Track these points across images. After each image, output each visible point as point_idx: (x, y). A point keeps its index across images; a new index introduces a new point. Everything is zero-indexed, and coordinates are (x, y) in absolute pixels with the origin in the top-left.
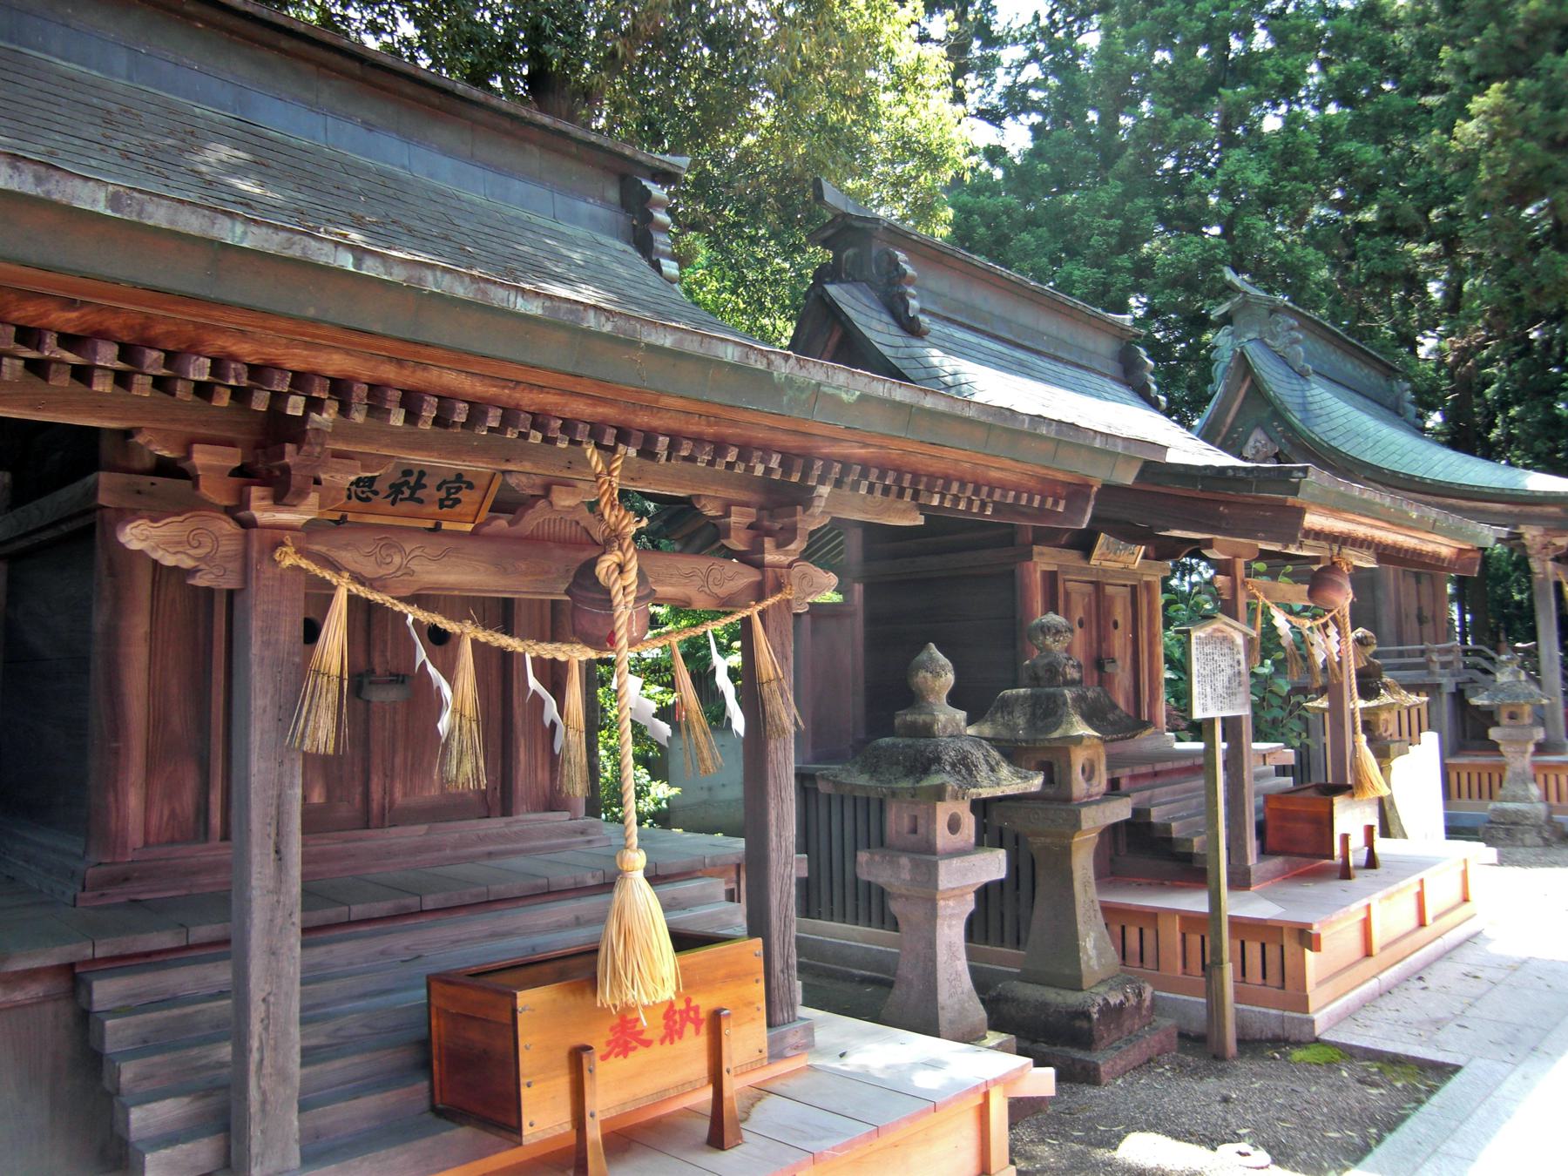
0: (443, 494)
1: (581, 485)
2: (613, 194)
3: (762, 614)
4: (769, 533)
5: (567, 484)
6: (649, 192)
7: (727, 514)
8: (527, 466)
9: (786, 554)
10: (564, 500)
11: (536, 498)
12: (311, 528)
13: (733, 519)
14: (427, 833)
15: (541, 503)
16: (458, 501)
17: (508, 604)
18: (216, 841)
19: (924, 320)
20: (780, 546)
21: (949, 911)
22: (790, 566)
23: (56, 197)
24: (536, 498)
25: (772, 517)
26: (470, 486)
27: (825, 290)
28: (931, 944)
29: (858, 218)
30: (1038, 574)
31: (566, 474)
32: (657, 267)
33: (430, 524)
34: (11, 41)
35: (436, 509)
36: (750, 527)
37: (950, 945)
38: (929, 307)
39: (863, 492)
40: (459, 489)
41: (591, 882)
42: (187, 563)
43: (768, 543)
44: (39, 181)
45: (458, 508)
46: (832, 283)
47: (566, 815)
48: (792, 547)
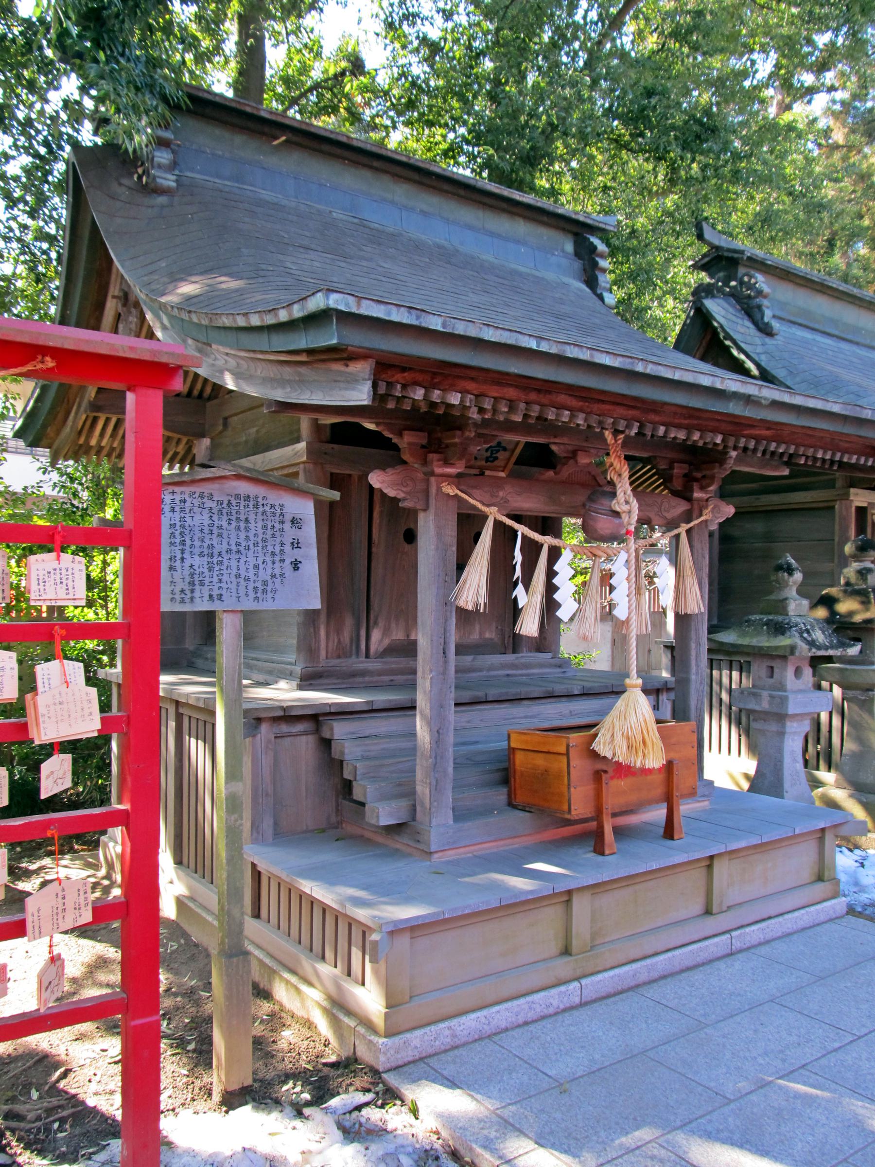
0: (489, 454)
1: (592, 451)
2: (569, 247)
3: (688, 532)
4: (697, 480)
5: (584, 450)
6: (595, 248)
7: (671, 468)
8: (565, 440)
9: (706, 493)
10: (583, 460)
11: (568, 458)
12: (459, 476)
13: (675, 471)
14: (473, 660)
15: (571, 462)
16: (496, 458)
17: (545, 519)
18: (363, 659)
19: (776, 325)
20: (702, 488)
21: (793, 730)
22: (707, 500)
23: (423, 325)
24: (568, 458)
25: (698, 469)
26: (505, 449)
27: (702, 304)
28: (780, 750)
29: (729, 250)
30: (853, 509)
31: (585, 444)
32: (601, 298)
33: (476, 472)
34: (237, 182)
35: (483, 463)
36: (685, 476)
37: (793, 752)
38: (778, 313)
39: (759, 455)
40: (498, 451)
41: (576, 692)
42: (401, 495)
43: (696, 486)
44: (418, 318)
45: (496, 463)
46: (706, 297)
47: (550, 655)
48: (711, 488)
